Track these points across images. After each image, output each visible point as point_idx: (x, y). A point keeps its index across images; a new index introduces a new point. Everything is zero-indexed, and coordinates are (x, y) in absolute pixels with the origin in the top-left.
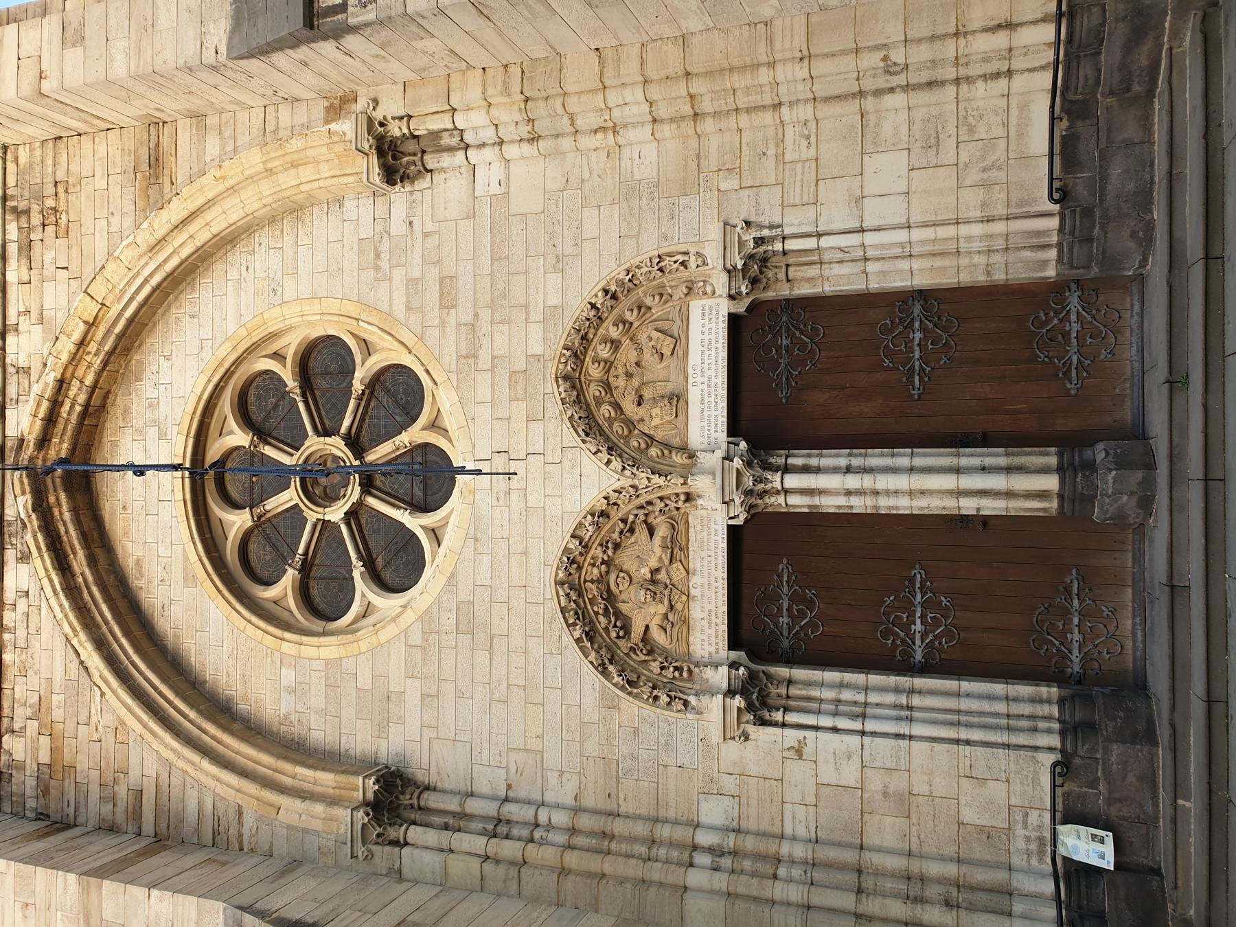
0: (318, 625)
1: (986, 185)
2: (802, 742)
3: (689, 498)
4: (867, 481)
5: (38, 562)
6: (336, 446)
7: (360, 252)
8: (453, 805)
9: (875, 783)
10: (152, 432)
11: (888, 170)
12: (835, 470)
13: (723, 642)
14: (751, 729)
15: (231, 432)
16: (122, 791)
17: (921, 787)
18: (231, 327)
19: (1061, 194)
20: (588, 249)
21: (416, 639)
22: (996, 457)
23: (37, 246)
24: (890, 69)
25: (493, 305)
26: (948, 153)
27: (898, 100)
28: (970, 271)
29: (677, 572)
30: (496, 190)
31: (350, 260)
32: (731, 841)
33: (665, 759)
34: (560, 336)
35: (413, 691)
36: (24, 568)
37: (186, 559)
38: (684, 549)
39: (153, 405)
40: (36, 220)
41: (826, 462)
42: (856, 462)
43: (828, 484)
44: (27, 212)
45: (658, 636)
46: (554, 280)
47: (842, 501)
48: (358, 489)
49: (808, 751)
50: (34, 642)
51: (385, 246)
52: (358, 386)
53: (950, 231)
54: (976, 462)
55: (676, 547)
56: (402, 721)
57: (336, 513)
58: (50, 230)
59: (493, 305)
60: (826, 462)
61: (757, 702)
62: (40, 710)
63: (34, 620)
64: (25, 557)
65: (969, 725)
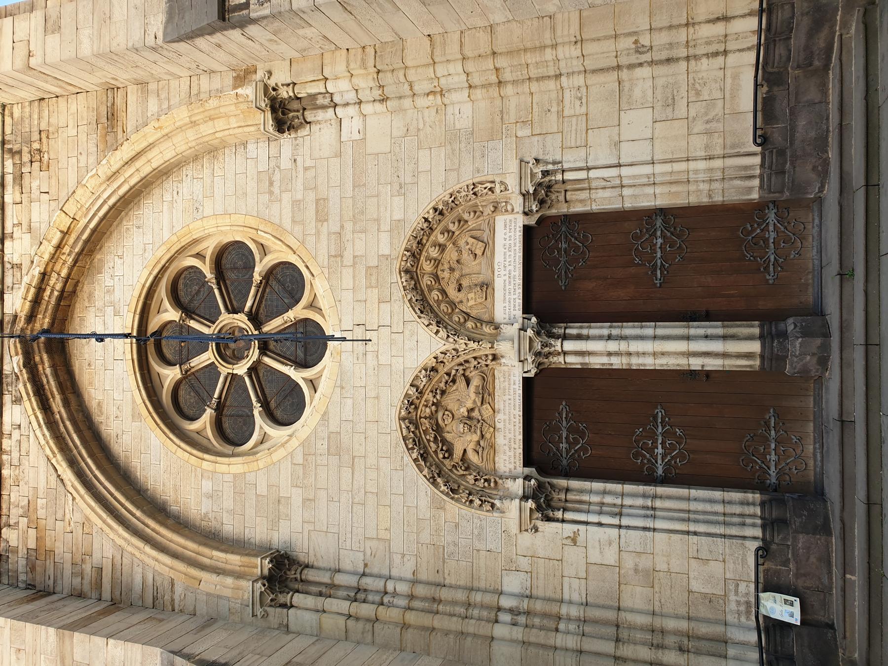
0: (229, 449)
1: (708, 133)
2: (576, 533)
3: (495, 358)
4: (623, 346)
5: (27, 404)
6: (241, 320)
7: (259, 181)
8: (325, 578)
9: (629, 563)
10: (110, 310)
11: (638, 122)
12: (600, 338)
13: (519, 461)
14: (539, 524)
15: (166, 311)
16: (87, 568)
17: (661, 566)
18: (166, 235)
19: (762, 139)
20: (422, 179)
21: (299, 459)
22: (716, 328)
23: (26, 177)
24: (639, 49)
25: (354, 219)
26: (681, 110)
27: (645, 71)
28: (697, 194)
29: (486, 411)
30: (356, 136)
31: (251, 187)
32: (525, 605)
33: (478, 545)
34: (402, 241)
35: (297, 497)
36: (17, 408)
37: (134, 401)
38: (492, 395)
39: (110, 291)
40: (26, 158)
41: (593, 332)
42: (615, 332)
43: (595, 348)
44: (20, 152)
45: (473, 457)
46: (398, 201)
47: (605, 360)
48: (257, 351)
49: (581, 539)
50: (24, 461)
51: (277, 177)
52: (257, 277)
53: (683, 166)
54: (701, 332)
55: (486, 393)
56: (289, 518)
57: (241, 369)
58: (36, 165)
59: (354, 219)
60: (593, 332)
61: (544, 504)
62: (29, 510)
63: (24, 445)
64: (18, 400)
65: (696, 521)
